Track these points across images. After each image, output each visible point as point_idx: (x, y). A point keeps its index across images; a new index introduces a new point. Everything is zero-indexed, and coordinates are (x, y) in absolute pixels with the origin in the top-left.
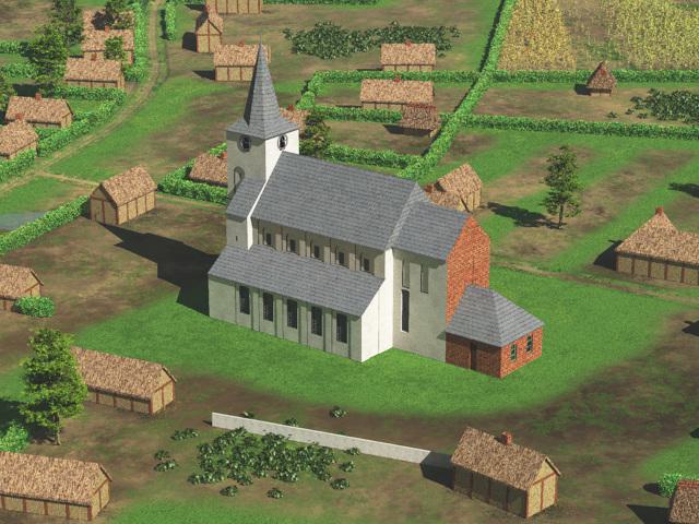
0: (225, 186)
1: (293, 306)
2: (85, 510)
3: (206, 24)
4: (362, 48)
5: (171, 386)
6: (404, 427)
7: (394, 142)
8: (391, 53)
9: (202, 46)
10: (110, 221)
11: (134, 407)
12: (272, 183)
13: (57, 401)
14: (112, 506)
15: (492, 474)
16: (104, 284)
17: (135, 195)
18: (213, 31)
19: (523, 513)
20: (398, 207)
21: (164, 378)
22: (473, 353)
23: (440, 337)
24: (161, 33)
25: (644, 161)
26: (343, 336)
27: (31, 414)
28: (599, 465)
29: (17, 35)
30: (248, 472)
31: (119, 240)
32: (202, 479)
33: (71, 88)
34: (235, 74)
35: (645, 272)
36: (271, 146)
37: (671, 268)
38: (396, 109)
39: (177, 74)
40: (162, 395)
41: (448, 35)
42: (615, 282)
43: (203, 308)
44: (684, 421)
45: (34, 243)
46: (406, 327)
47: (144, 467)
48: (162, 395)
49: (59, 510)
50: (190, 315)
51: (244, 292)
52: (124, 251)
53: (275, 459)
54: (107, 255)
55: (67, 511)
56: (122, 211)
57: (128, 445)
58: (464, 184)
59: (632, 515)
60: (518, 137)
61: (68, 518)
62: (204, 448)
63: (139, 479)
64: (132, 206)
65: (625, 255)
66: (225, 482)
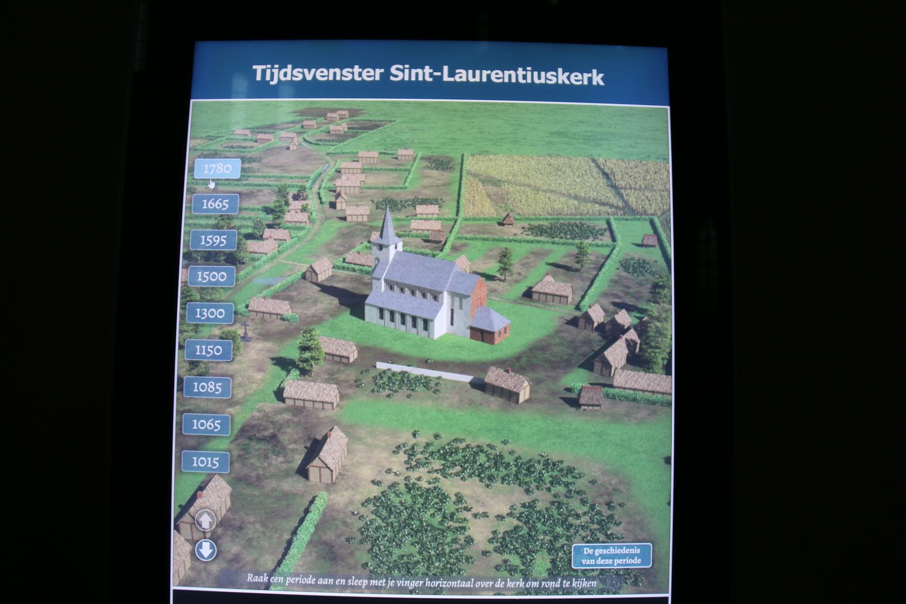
0: (371, 266)
1: (403, 316)
2: (330, 405)
3: (340, 198)
4: (405, 207)
5: (357, 351)
6: (461, 367)
7: (427, 246)
8: (420, 209)
9: (338, 206)
10: (314, 280)
11: (341, 360)
12: (392, 265)
13: (313, 358)
14: (341, 403)
15: (503, 386)
16: (317, 308)
17: (325, 270)
18: (343, 200)
19: (517, 402)
20: (449, 273)
21: (354, 348)
22: (482, 335)
23: (467, 328)
24: (319, 202)
25: (533, 253)
26: (426, 328)
27: (301, 364)
28: (544, 381)
29: (260, 203)
30: (396, 387)
31: (319, 289)
32: (377, 391)
33: (289, 225)
34: (355, 218)
35: (544, 299)
36: (392, 247)
37: (555, 298)
38: (426, 233)
39: (330, 218)
40: (353, 356)
41: (440, 202)
42: (532, 304)
43: (361, 316)
44: (574, 361)
45: (283, 291)
46: (452, 324)
47: (351, 386)
48: (353, 356)
49: (319, 406)
50: (361, 321)
51: (381, 310)
52: (322, 294)
53: (404, 379)
54: (316, 295)
55: (323, 406)
56: (319, 276)
57: (342, 377)
58: (463, 263)
59: (562, 401)
60: (479, 244)
61: (323, 409)
62: (375, 378)
63: (350, 391)
64: (323, 274)
65: (536, 292)
66: (387, 392)
